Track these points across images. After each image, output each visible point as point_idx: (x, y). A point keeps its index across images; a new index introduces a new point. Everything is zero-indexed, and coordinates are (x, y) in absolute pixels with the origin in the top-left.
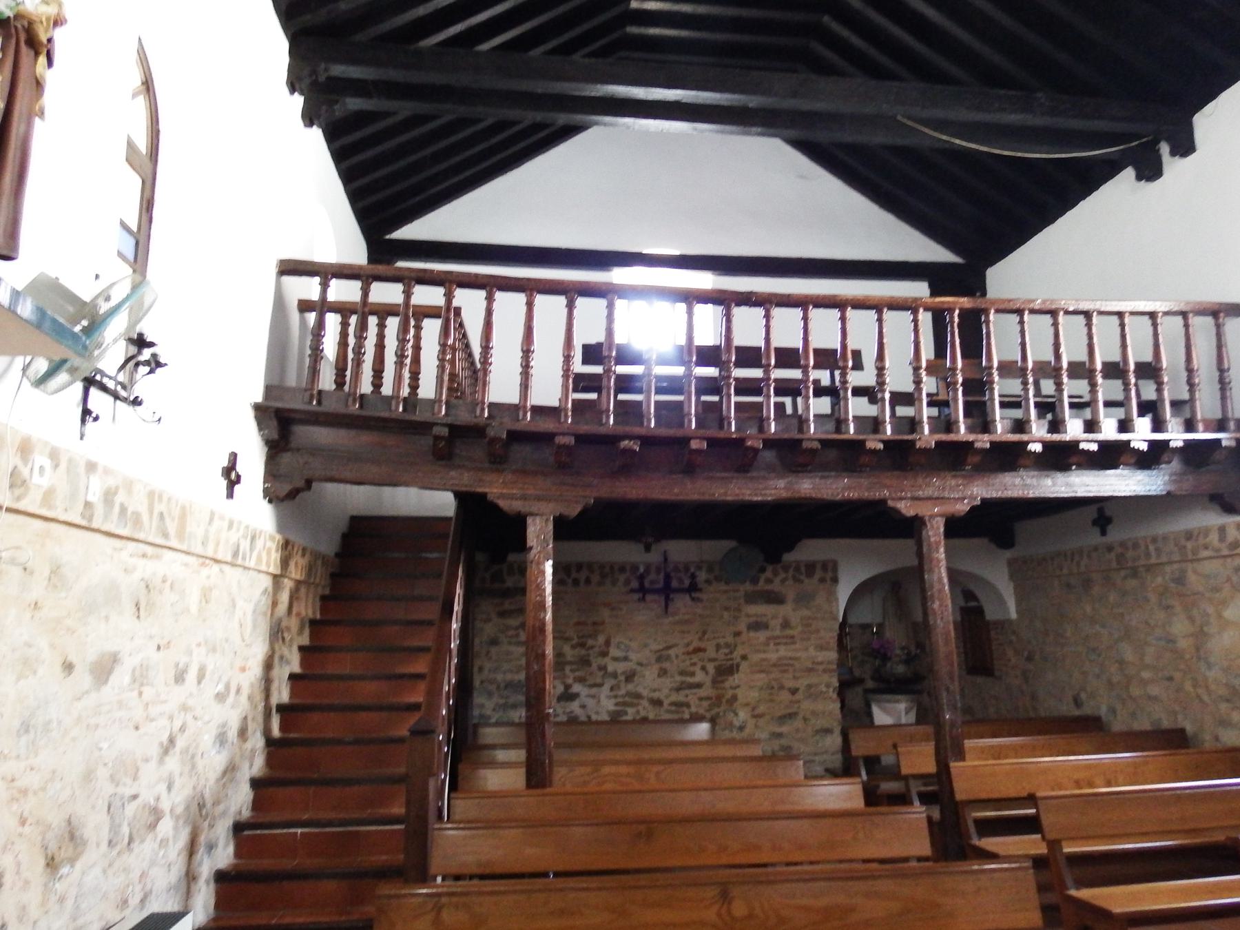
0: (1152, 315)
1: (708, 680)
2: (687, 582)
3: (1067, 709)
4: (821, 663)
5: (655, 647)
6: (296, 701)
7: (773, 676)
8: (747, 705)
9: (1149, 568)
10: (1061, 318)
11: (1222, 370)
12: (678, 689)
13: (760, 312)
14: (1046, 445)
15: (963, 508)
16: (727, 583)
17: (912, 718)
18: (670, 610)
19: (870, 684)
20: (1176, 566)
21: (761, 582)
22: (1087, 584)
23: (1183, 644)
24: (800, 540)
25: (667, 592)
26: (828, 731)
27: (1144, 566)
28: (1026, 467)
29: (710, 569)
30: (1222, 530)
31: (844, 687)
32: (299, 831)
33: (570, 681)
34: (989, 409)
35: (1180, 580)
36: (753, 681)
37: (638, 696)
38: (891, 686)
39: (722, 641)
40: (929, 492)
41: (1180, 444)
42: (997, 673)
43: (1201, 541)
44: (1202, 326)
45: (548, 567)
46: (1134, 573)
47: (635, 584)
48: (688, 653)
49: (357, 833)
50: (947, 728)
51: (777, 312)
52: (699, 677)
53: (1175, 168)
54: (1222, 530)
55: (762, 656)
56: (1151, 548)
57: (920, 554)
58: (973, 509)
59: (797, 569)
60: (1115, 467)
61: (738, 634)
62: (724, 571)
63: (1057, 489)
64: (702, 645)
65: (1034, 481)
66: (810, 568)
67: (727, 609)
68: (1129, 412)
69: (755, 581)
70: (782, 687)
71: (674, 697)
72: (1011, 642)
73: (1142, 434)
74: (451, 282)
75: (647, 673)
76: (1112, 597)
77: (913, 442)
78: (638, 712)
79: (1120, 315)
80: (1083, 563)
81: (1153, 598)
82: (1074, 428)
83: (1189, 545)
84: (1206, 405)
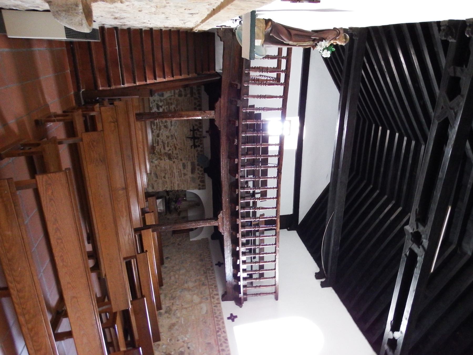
0: (275, 277)
1: (166, 151)
2: (197, 144)
3: (165, 255)
4: (174, 185)
5: (176, 134)
6: (154, 32)
7: (169, 171)
8: (159, 163)
9: (206, 277)
10: (274, 254)
11: (260, 294)
12: (163, 142)
13: (276, 175)
14: (238, 251)
15: (221, 230)
16: (197, 157)
17: (159, 211)
18: (188, 139)
19: (168, 197)
20: (207, 283)
21: (198, 167)
22: (202, 260)
23: (186, 285)
24: (211, 178)
25: (194, 138)
26: (153, 188)
27: (207, 275)
28: (232, 246)
29: (201, 151)
30: (217, 295)
31: (167, 192)
32: (117, 48)
33: (163, 107)
34: (248, 237)
35: (203, 284)
36: (167, 165)
37: (160, 130)
38: (167, 204)
39: (179, 155)
40: (225, 222)
41: (239, 284)
42: (174, 235)
43: (214, 289)
44: (272, 289)
45: (200, 118)
46: (205, 273)
47: (196, 128)
48: (174, 145)
49: (119, 66)
50: (160, 228)
51: (276, 180)
52: (167, 149)
53: (318, 282)
54: (217, 295)
55: (175, 168)
56: (212, 277)
57: (208, 219)
58: (221, 233)
59: (202, 178)
60: (233, 268)
61: (181, 160)
62: (201, 156)
63: (227, 254)
64: (177, 149)
65: (229, 248)
66: (203, 181)
67: (189, 156)
68: (248, 271)
69: (198, 165)
70: (165, 174)
71: (160, 141)
72: (183, 239)
73: (242, 275)
74: (285, 85)
75: (167, 132)
76: (198, 267)
77: (238, 218)
78: (155, 130)
79: (275, 269)
80: (207, 259)
81: (198, 278)
82: (243, 258)
83: (213, 287)
84: (251, 290)
